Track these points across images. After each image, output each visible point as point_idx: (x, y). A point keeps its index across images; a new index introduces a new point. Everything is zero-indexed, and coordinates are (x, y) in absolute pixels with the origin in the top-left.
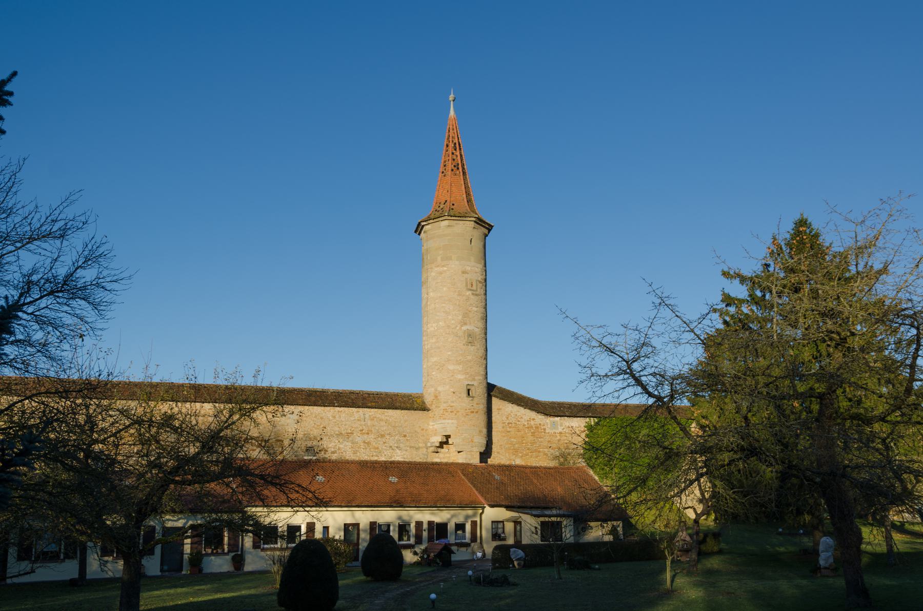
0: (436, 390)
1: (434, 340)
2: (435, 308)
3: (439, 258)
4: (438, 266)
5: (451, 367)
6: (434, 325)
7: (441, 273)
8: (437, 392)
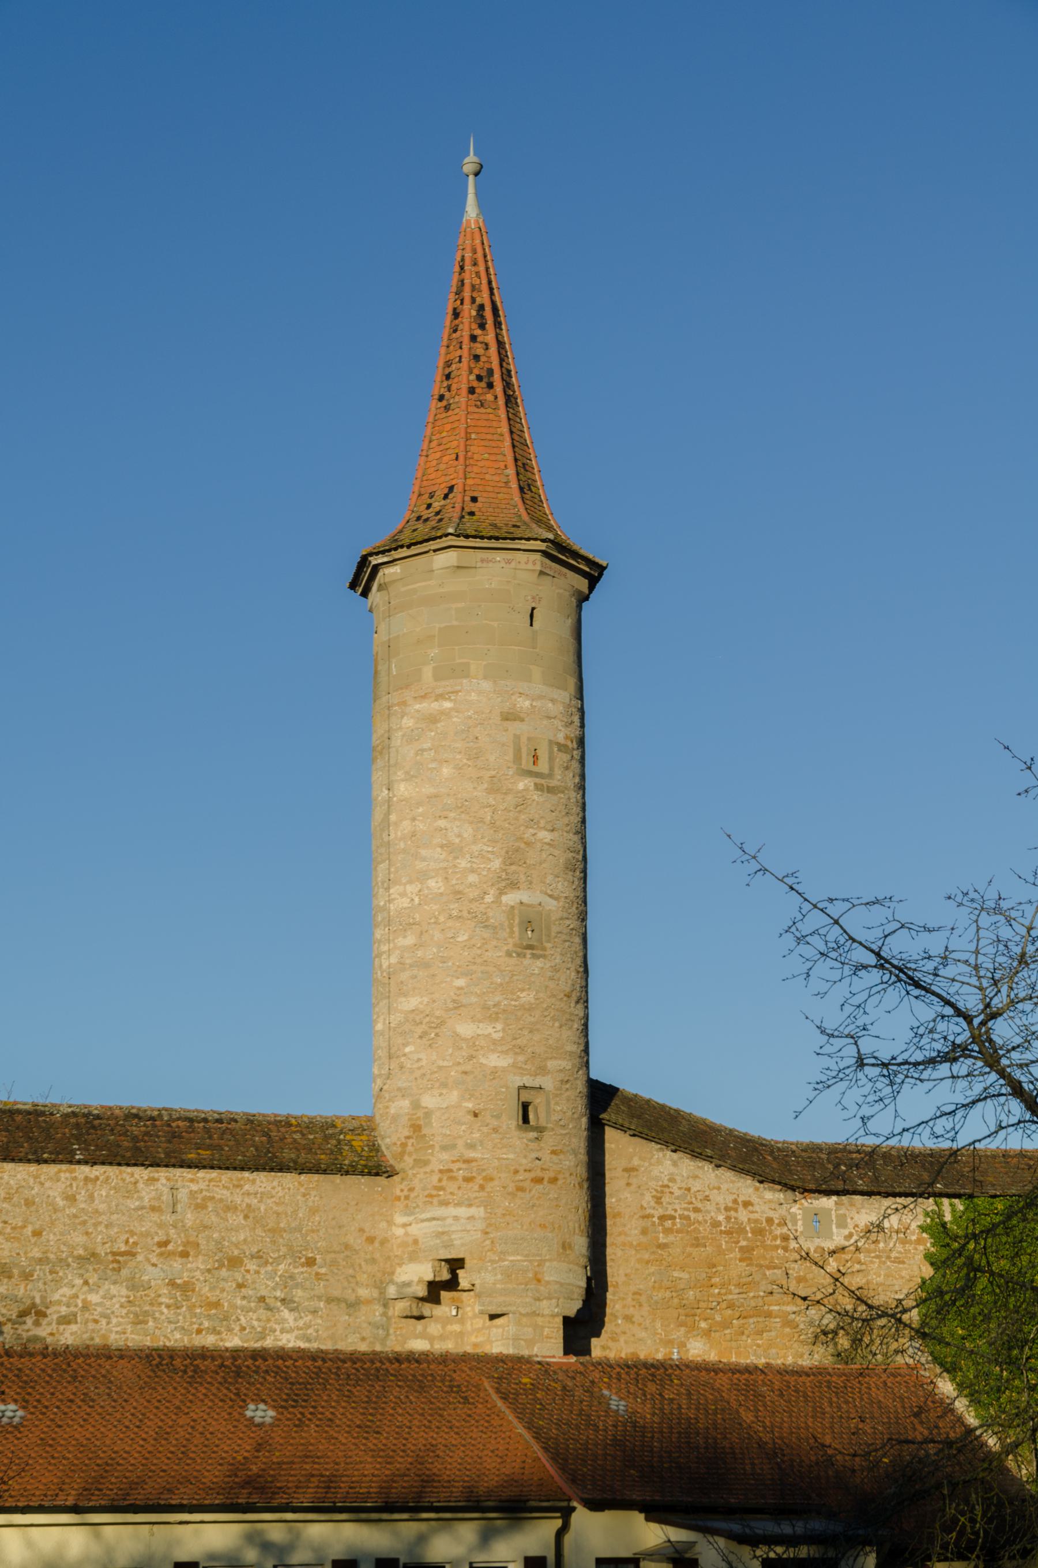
2: (413, 834)
3: (428, 672)
4: (424, 697)
7: (433, 719)
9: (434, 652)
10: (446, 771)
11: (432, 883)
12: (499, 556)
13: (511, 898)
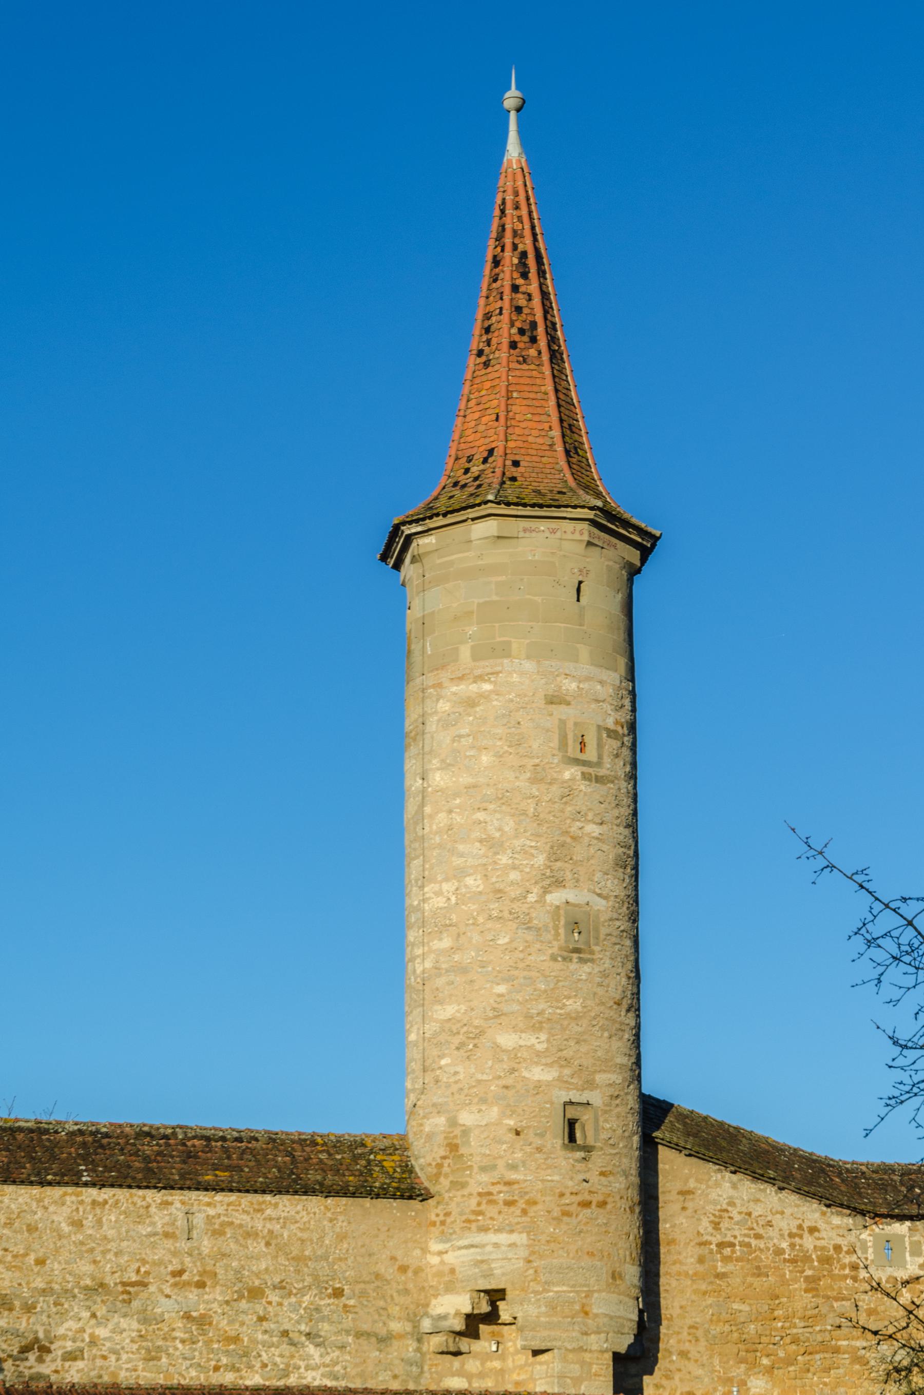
0: (453, 1122)
1: (446, 943)
2: (450, 828)
3: (465, 652)
4: (461, 678)
5: (507, 1040)
6: (446, 887)
7: (471, 703)
8: (457, 1131)
9: (472, 630)
10: (485, 759)
11: (470, 881)
12: (543, 525)
13: (556, 898)
